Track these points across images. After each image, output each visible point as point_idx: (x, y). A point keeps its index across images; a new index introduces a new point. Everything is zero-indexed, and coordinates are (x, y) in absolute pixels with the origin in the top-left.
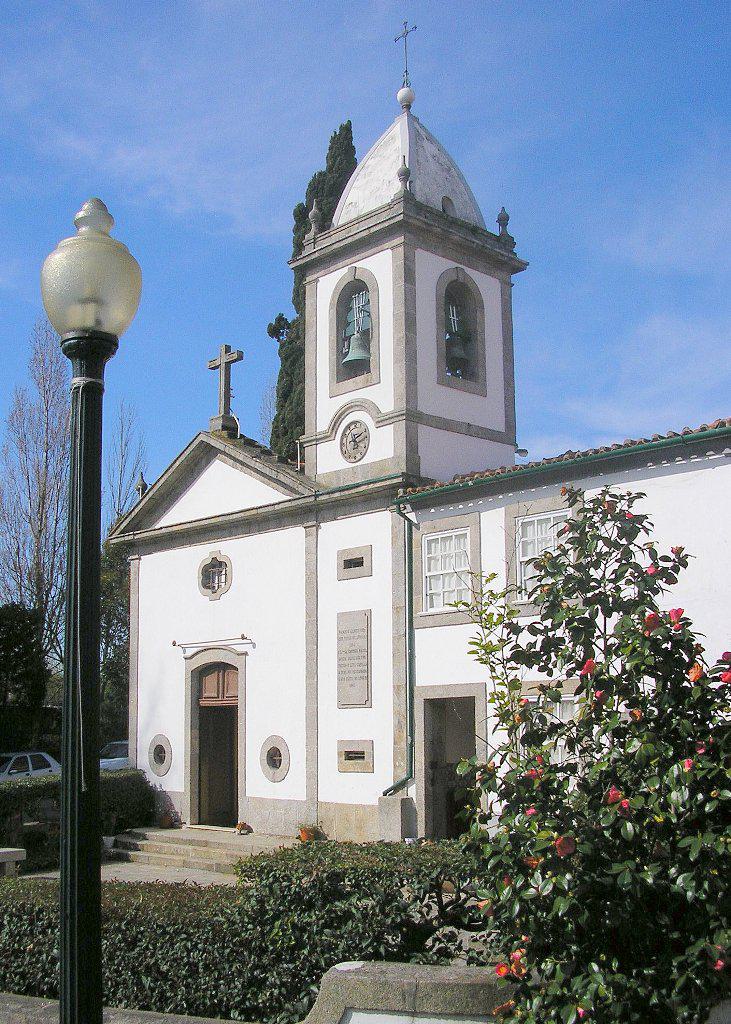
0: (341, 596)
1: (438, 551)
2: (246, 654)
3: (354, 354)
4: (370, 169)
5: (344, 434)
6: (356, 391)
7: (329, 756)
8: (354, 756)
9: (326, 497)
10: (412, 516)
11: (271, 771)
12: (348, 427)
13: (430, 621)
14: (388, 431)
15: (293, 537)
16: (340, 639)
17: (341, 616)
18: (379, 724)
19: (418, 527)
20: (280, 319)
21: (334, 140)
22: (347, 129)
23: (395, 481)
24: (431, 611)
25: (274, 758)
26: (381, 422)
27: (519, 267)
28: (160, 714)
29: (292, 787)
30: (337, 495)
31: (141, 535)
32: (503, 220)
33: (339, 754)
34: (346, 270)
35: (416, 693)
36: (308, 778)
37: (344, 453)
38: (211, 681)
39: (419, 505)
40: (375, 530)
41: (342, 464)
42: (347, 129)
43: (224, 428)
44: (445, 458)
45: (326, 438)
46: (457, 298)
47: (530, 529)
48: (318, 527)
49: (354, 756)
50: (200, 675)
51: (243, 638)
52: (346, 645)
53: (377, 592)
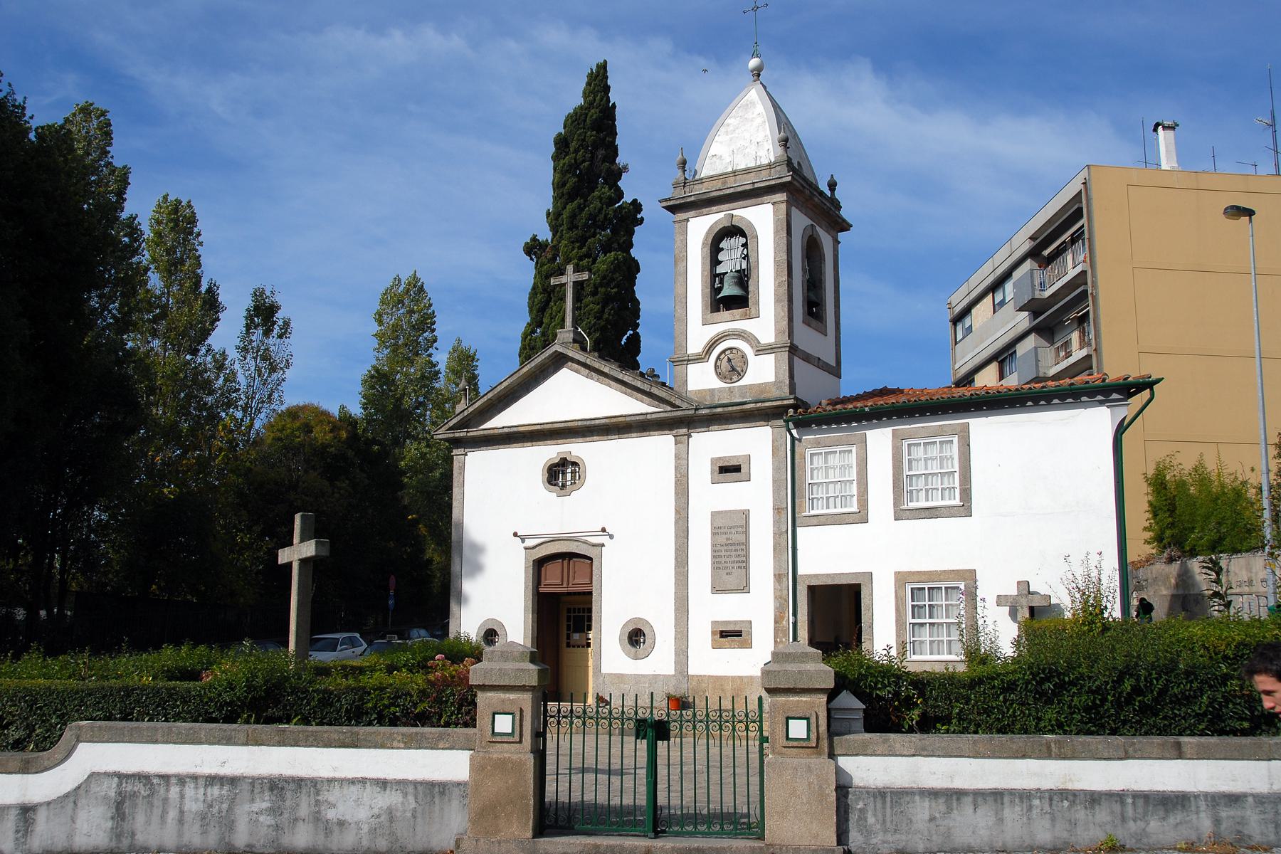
0: (710, 498)
1: (919, 453)
2: (603, 545)
3: (729, 290)
4: (731, 128)
5: (718, 358)
6: (729, 322)
7: (700, 635)
8: (730, 635)
9: (707, 411)
10: (794, 432)
11: (633, 650)
12: (723, 352)
13: (815, 520)
14: (770, 359)
15: (663, 443)
16: (714, 534)
17: (714, 514)
18: (758, 606)
19: (800, 440)
20: (534, 239)
21: (591, 75)
22: (603, 67)
23: (786, 402)
24: (813, 512)
25: (636, 637)
26: (762, 350)
27: (845, 226)
28: (494, 601)
29: (659, 662)
30: (719, 410)
31: (473, 433)
32: (832, 186)
33: (713, 633)
34: (721, 215)
35: (799, 580)
36: (677, 654)
37: (718, 374)
38: (552, 571)
39: (803, 424)
40: (756, 443)
41: (717, 384)
42: (603, 67)
43: (575, 341)
44: (816, 389)
45: (701, 358)
46: (812, 250)
47: (815, 458)
48: (689, 436)
49: (730, 635)
50: (539, 565)
51: (604, 530)
52: (722, 539)
53: (756, 496)
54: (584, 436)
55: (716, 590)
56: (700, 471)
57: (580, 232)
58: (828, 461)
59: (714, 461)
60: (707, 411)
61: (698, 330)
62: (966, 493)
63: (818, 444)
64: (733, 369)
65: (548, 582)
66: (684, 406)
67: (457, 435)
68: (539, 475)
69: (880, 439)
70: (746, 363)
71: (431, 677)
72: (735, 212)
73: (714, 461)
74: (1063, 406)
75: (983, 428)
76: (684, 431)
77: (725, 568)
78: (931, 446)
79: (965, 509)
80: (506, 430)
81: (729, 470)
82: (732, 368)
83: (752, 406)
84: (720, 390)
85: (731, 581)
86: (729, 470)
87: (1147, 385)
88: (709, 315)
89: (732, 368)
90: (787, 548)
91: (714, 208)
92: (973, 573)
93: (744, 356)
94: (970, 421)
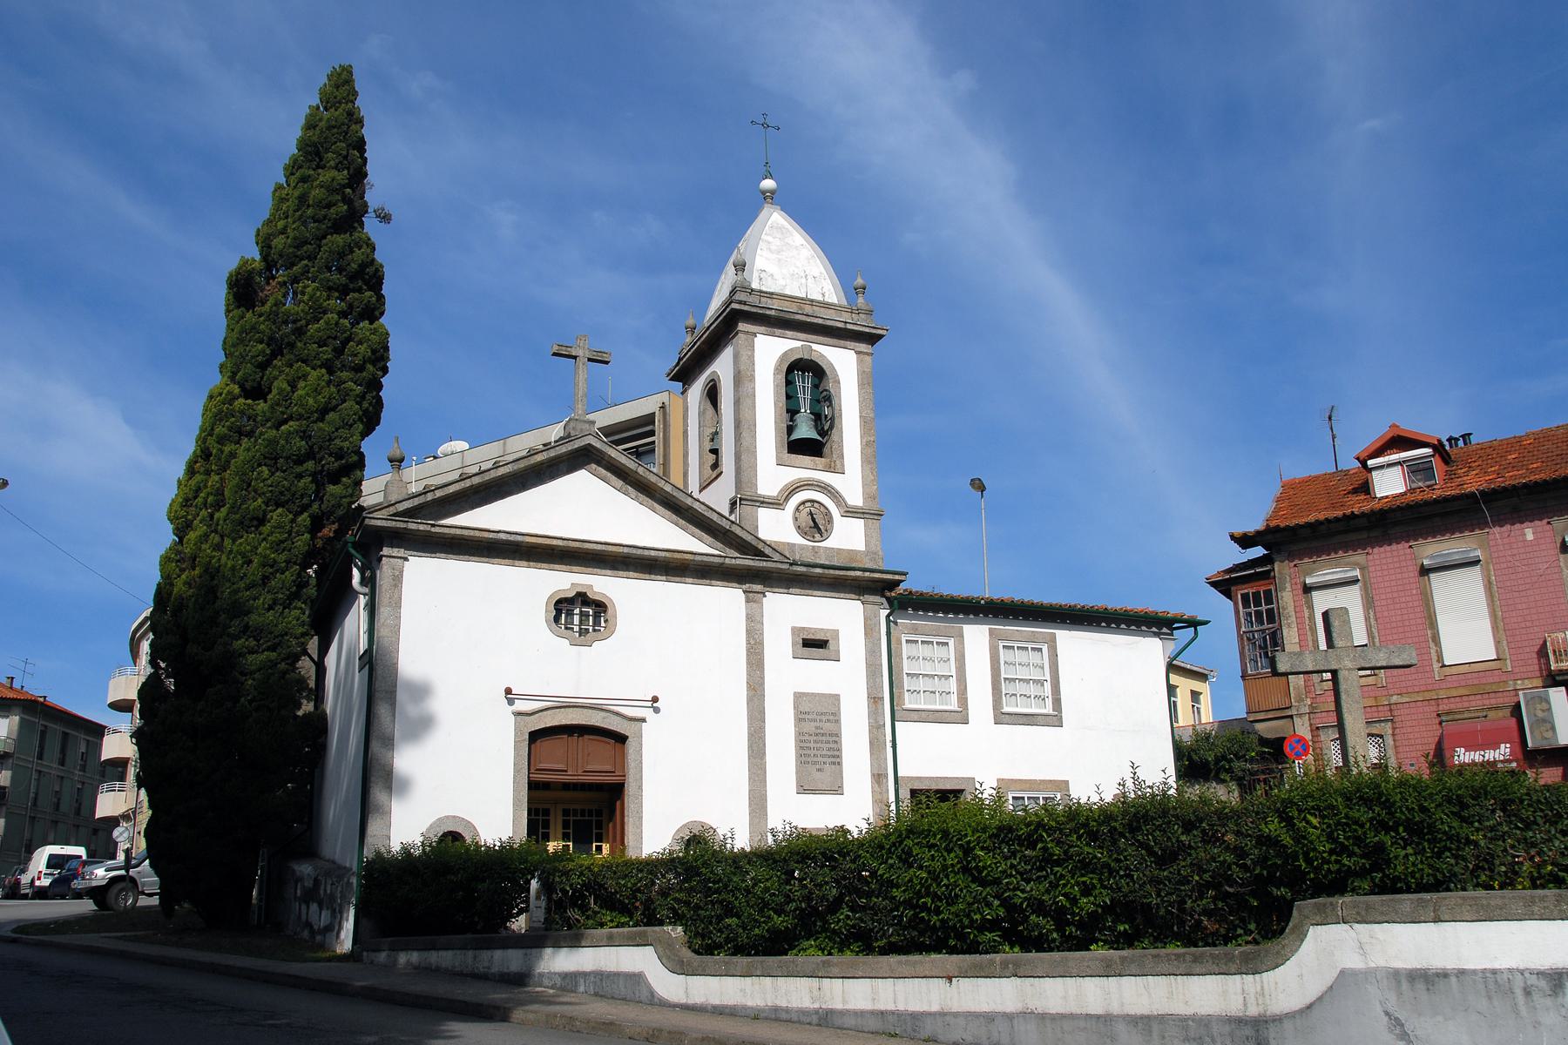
0: (790, 676)
2: (644, 720)
3: (805, 430)
9: (803, 569)
13: (915, 716)
15: (728, 599)
26: (851, 512)
30: (818, 570)
34: (799, 344)
40: (843, 616)
45: (776, 503)
52: (809, 727)
53: (845, 678)
54: (614, 568)
55: (803, 789)
56: (778, 645)
57: (344, 280)
58: (924, 652)
59: (795, 631)
60: (803, 569)
61: (773, 472)
62: (1057, 703)
63: (915, 630)
64: (816, 525)
65: (543, 766)
66: (776, 557)
67: (412, 526)
68: (540, 612)
69: (977, 635)
70: (830, 520)
71: (1189, 860)
72: (814, 346)
73: (795, 631)
74: (1118, 631)
75: (1071, 642)
76: (758, 587)
77: (815, 763)
78: (1025, 652)
79: (1055, 720)
80: (503, 536)
81: (814, 644)
82: (816, 525)
83: (859, 573)
84: (802, 547)
85: (824, 778)
86: (814, 644)
87: (1194, 623)
88: (786, 456)
89: (816, 525)
90: (882, 745)
91: (789, 333)
92: (1067, 782)
93: (828, 514)
94: (1057, 632)
